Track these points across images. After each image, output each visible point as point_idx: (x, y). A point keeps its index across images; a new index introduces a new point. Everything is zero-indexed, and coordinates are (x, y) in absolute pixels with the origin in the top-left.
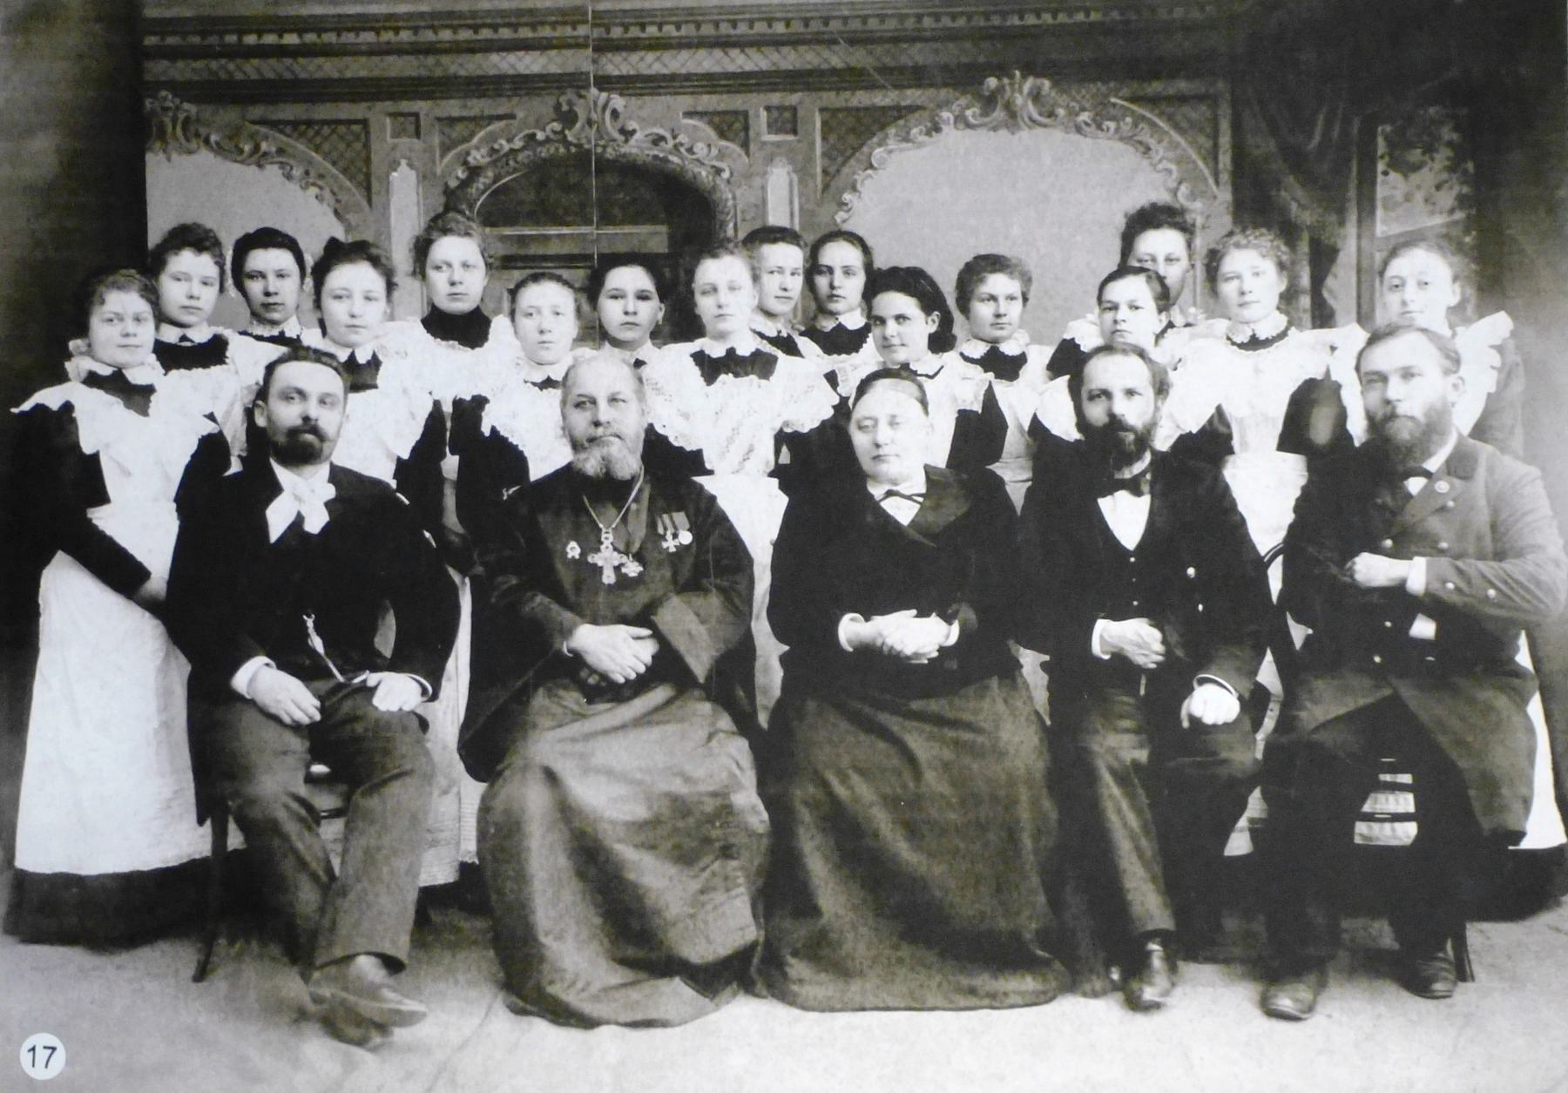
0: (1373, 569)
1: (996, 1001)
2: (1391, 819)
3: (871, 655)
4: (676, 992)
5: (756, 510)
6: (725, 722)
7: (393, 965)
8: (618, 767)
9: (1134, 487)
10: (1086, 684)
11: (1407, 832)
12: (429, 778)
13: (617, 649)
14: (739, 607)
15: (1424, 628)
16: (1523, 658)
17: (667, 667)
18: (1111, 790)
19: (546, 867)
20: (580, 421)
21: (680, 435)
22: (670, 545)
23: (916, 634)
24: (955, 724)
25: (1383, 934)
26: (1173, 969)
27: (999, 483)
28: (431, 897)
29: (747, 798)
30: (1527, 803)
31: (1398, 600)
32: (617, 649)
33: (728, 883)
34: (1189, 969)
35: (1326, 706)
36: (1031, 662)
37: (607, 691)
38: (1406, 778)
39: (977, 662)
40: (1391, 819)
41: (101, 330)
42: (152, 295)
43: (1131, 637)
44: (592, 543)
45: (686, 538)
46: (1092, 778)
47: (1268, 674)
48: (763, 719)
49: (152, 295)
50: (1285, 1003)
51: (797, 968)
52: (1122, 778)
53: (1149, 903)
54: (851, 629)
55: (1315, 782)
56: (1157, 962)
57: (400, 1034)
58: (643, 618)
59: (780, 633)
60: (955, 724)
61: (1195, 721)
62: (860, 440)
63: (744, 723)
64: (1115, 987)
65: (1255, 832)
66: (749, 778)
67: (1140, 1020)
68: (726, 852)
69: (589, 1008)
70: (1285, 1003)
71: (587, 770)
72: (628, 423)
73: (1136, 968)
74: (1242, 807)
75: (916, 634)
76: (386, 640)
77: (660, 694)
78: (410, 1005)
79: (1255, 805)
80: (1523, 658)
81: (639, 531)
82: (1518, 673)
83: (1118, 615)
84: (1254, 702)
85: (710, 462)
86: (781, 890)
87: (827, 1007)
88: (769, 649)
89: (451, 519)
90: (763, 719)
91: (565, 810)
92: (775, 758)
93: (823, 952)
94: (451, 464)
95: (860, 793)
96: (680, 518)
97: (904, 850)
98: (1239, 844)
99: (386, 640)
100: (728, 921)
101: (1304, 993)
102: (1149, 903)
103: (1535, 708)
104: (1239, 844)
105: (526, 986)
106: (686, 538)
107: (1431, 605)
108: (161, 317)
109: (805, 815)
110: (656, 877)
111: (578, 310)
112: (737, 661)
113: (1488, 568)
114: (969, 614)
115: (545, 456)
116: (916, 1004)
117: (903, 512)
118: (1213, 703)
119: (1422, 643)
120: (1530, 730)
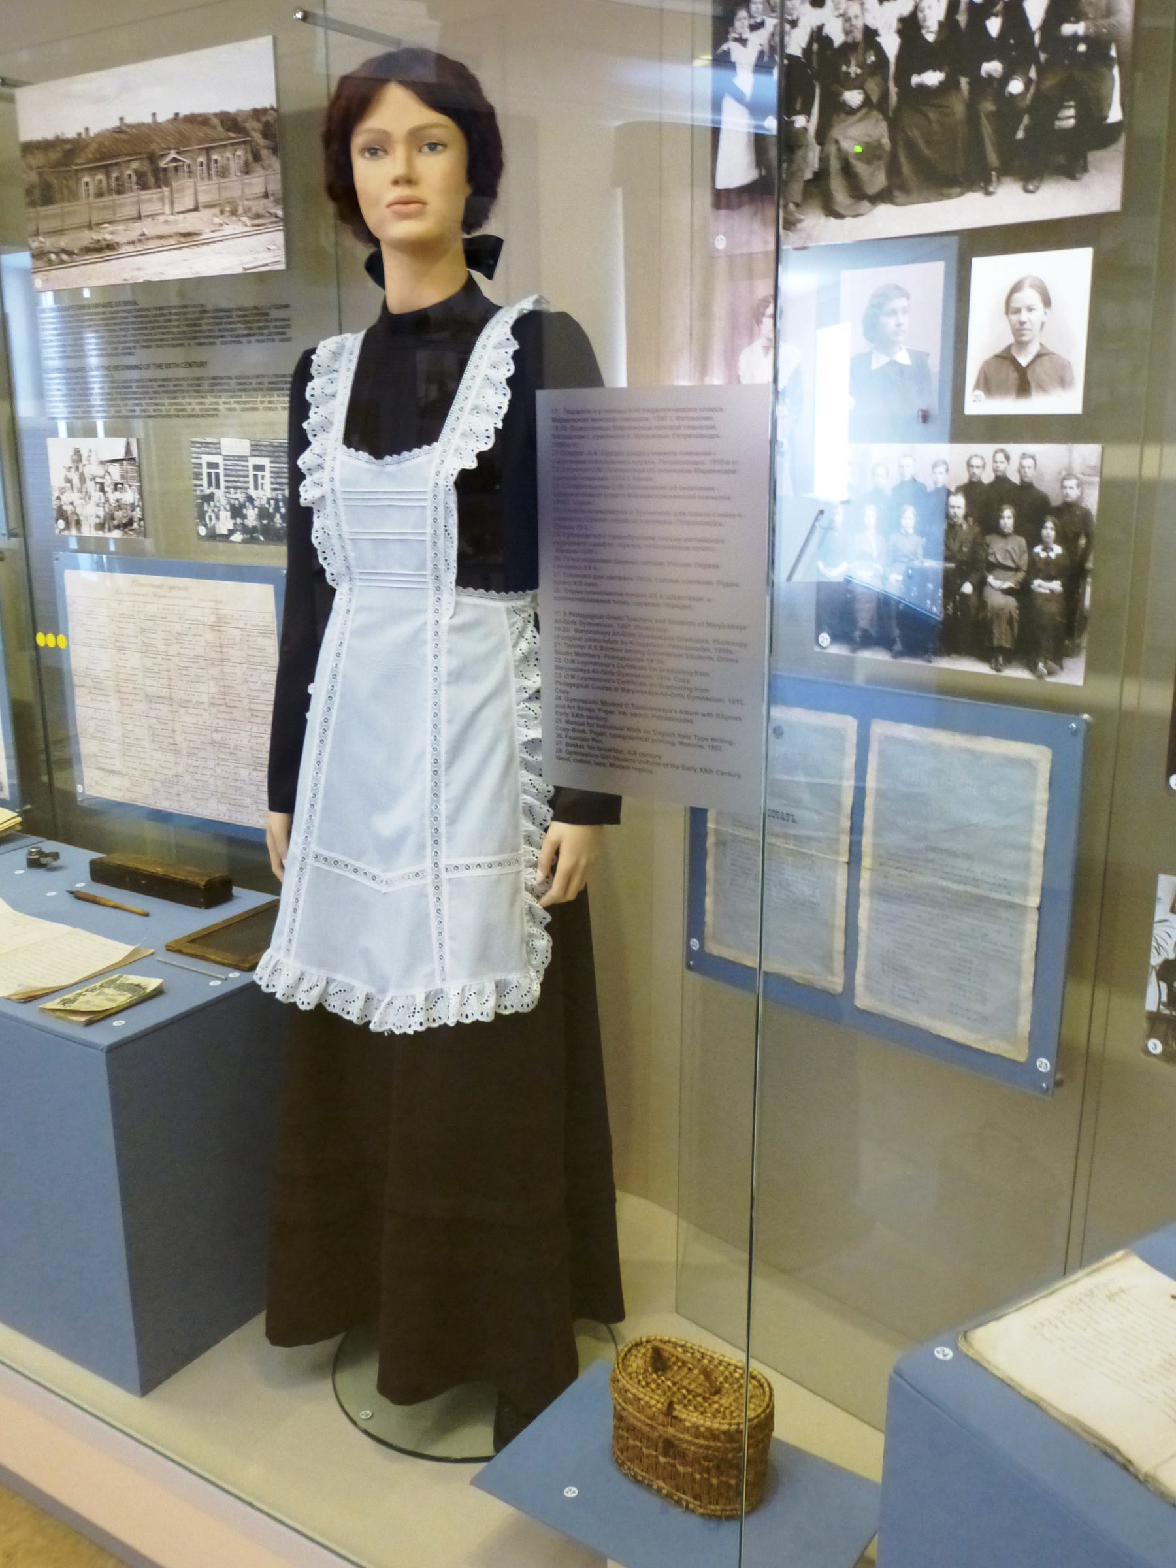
0: (1068, 29)
1: (949, 197)
2: (1068, 118)
3: (922, 87)
4: (866, 204)
5: (891, 44)
6: (881, 117)
7: (797, 205)
8: (854, 137)
9: (996, 15)
10: (982, 85)
11: (1072, 122)
12: (807, 146)
13: (854, 97)
14: (885, 79)
15: (1082, 48)
16: (1113, 53)
17: (867, 102)
18: (985, 122)
19: (835, 165)
20: (847, 25)
21: (872, 24)
22: (869, 62)
23: (932, 78)
24: (940, 106)
25: (1062, 159)
26: (998, 179)
27: (957, 21)
28: (808, 182)
29: (886, 141)
30: (1110, 106)
31: (1075, 39)
32: (854, 97)
33: (879, 168)
34: (1004, 179)
35: (1050, 82)
36: (964, 81)
37: (851, 111)
38: (1072, 103)
39: (949, 85)
40: (1068, 118)
41: (737, 24)
42: (749, 11)
43: (992, 68)
44: (848, 66)
45: (873, 58)
46: (979, 117)
47: (1033, 74)
48: (890, 114)
49: (749, 11)
50: (1031, 187)
51: (897, 193)
52: (987, 116)
53: (993, 158)
54: (915, 79)
55: (1044, 106)
56: (994, 179)
57: (799, 226)
58: (860, 87)
59: (896, 85)
60: (940, 106)
61: (1011, 94)
62: (920, 15)
63: (886, 118)
64: (982, 188)
65: (1027, 130)
66: (886, 134)
67: (989, 198)
68: (879, 158)
69: (842, 211)
70: (1031, 187)
71: (846, 137)
72: (859, 23)
73: (988, 181)
74: (1021, 120)
75: (932, 78)
76: (798, 106)
77: (864, 111)
78: (801, 217)
79: (1026, 120)
80: (1113, 53)
81: (860, 58)
82: (1112, 58)
83: (989, 60)
84: (1028, 83)
85: (881, 31)
86: (893, 170)
87: (904, 205)
88: (893, 89)
89: (815, 65)
90: (890, 114)
91: (839, 150)
92: (894, 126)
93: (905, 189)
94: (815, 47)
95: (915, 133)
96: (872, 52)
97: (927, 152)
98: (1020, 134)
99: (798, 106)
100: (876, 179)
101: (1036, 183)
102: (993, 158)
103: (1116, 71)
104: (1020, 134)
105: (831, 211)
106: (873, 58)
107: (1085, 39)
108: (751, 16)
109: (901, 143)
110: (860, 168)
111: (773, 35)
112: (885, 94)
113: (1102, 22)
114: (947, 68)
115: (838, 39)
116: (927, 200)
117: (930, 38)
118: (1016, 86)
119: (1081, 53)
120: (1113, 78)
